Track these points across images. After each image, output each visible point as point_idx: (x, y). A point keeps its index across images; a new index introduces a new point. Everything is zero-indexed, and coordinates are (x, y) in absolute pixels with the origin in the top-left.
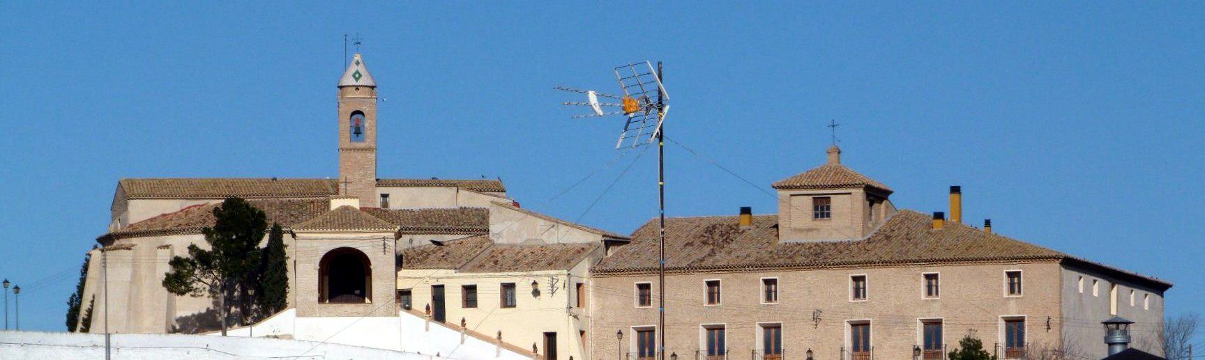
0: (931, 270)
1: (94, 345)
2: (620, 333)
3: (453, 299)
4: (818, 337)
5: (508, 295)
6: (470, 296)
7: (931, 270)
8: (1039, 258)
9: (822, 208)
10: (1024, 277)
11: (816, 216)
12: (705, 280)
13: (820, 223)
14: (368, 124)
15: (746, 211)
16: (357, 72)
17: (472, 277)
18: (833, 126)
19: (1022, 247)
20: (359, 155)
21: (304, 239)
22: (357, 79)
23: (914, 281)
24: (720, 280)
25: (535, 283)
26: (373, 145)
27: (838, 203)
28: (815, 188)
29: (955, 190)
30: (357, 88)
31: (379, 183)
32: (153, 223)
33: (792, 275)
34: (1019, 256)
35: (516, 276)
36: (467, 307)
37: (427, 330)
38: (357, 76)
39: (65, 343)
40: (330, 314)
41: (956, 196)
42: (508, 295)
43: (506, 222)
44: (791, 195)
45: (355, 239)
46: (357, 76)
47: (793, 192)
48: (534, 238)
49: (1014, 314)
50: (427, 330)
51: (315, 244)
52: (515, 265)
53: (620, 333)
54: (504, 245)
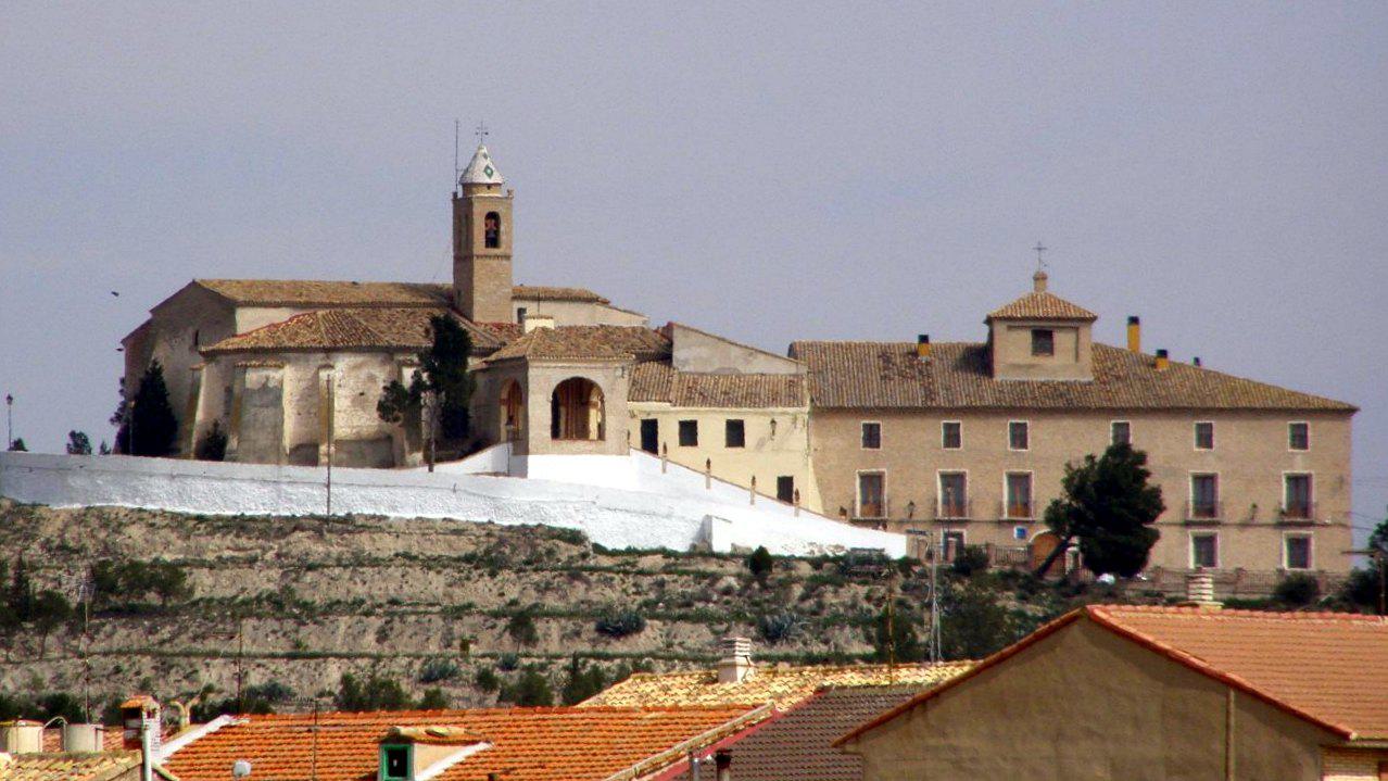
3: (668, 433)
5: (735, 435)
6: (689, 433)
13: (1041, 360)
15: (924, 339)
16: (487, 167)
19: (1249, 387)
20: (494, 263)
22: (490, 176)
29: (1134, 321)
31: (518, 297)
32: (1029, 395)
35: (745, 413)
38: (489, 171)
39: (247, 475)
40: (562, 452)
41: (1134, 327)
43: (693, 348)
46: (489, 171)
47: (1012, 324)
49: (1299, 470)
52: (706, 399)
53: (10, 398)
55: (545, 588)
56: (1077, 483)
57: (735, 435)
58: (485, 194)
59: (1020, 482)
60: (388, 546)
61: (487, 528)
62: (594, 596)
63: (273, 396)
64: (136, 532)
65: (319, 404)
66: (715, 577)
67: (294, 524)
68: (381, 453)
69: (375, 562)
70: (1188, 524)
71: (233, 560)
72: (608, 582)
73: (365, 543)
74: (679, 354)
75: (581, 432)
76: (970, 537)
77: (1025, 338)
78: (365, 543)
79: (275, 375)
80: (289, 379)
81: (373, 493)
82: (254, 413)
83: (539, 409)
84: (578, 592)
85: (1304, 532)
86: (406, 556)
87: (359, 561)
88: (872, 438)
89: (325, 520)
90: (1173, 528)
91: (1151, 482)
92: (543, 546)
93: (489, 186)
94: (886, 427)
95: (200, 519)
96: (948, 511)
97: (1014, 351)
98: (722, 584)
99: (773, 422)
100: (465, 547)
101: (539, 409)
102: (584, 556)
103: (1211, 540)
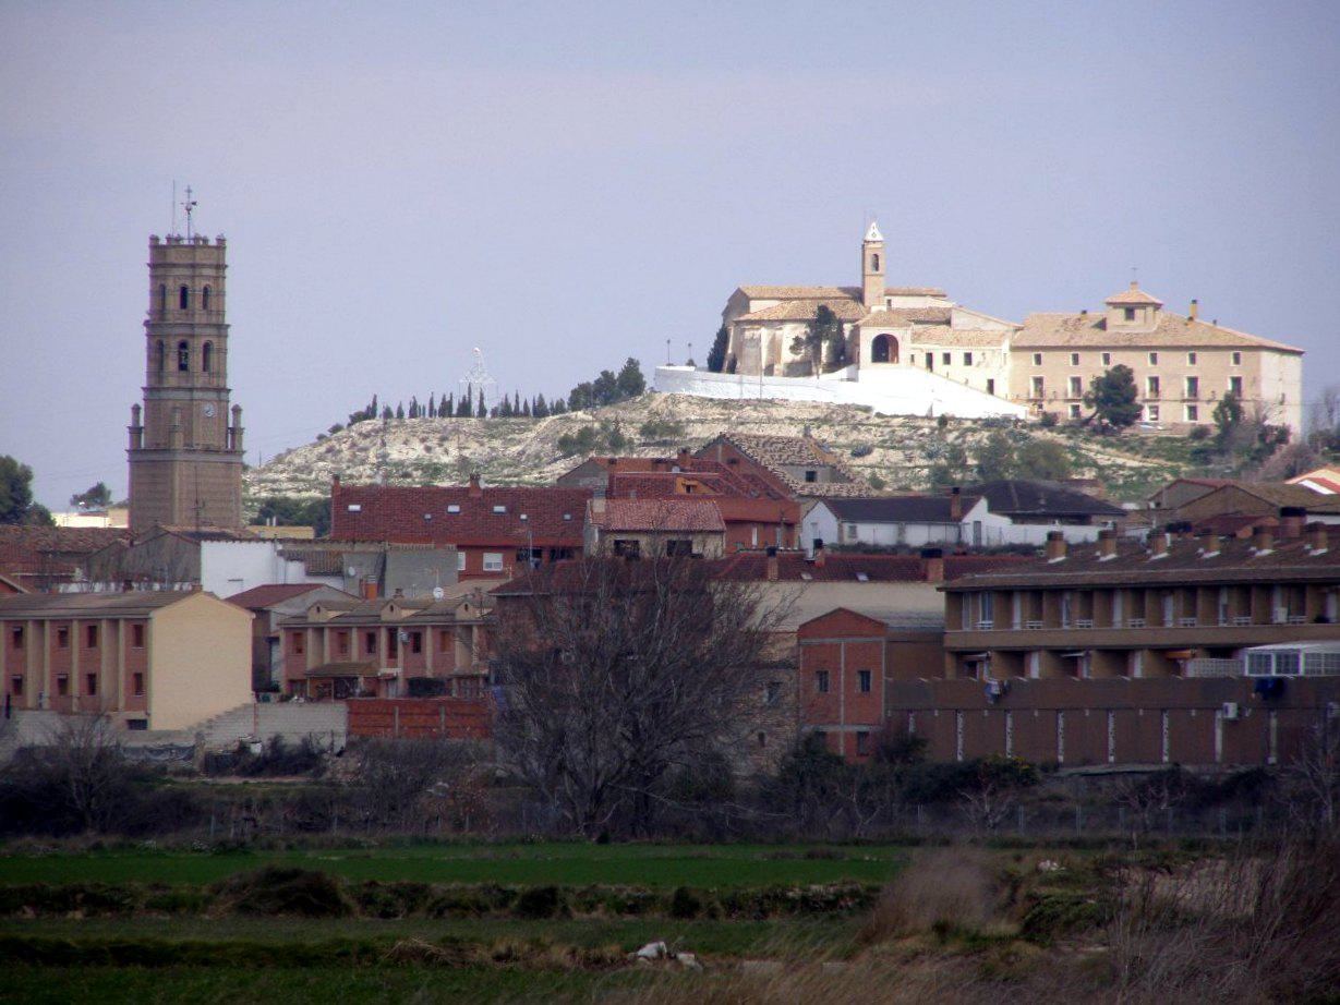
3: (938, 360)
5: (968, 359)
6: (947, 358)
13: (1129, 323)
29: (1194, 302)
55: (838, 434)
56: (1098, 383)
57: (968, 359)
58: (872, 245)
59: (1076, 381)
60: (782, 413)
61: (828, 405)
62: (860, 437)
63: (757, 342)
64: (683, 406)
65: (775, 346)
66: (919, 428)
67: (748, 402)
68: (801, 369)
69: (776, 421)
70: (1184, 401)
71: (718, 419)
72: (869, 431)
73: (774, 412)
74: (953, 322)
75: (886, 360)
76: (1047, 407)
77: (1121, 312)
78: (774, 412)
79: (757, 333)
80: (764, 334)
81: (783, 389)
82: (749, 350)
83: (866, 350)
84: (854, 435)
85: (1156, 404)
86: (791, 419)
87: (771, 420)
88: (1038, 359)
89: (759, 400)
90: (1174, 404)
91: (1134, 383)
92: (851, 413)
93: (874, 242)
94: (1243, 354)
95: (711, 400)
96: (1190, 395)
97: (1117, 317)
98: (920, 432)
99: (983, 354)
100: (817, 413)
101: (866, 350)
102: (868, 418)
103: (1157, 407)
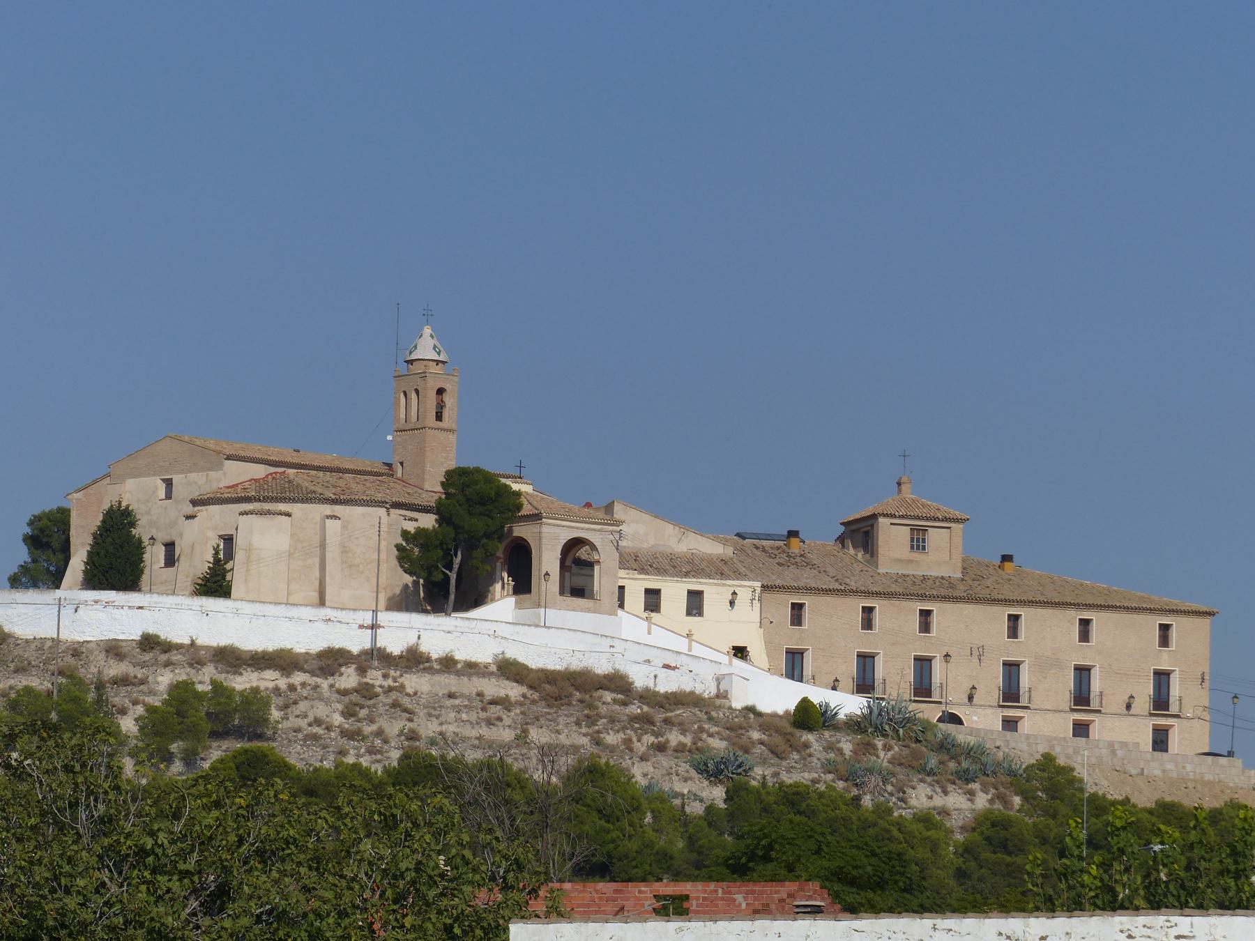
0: (1086, 615)
1: (329, 619)
2: (947, 655)
4: (975, 674)
5: (695, 603)
7: (1086, 615)
8: (1075, 605)
9: (918, 542)
10: (1176, 631)
11: (912, 547)
12: (861, 605)
13: (916, 556)
14: (449, 400)
17: (657, 580)
18: (905, 456)
21: (550, 524)
23: (1069, 624)
24: (1094, 618)
25: (734, 593)
26: (454, 427)
27: (936, 537)
28: (935, 520)
30: (438, 362)
33: (949, 607)
34: (1144, 606)
36: (86, 589)
37: (649, 633)
42: (695, 603)
44: (891, 524)
45: (587, 529)
48: (662, 543)
50: (649, 633)
51: (557, 530)
54: (628, 548)
